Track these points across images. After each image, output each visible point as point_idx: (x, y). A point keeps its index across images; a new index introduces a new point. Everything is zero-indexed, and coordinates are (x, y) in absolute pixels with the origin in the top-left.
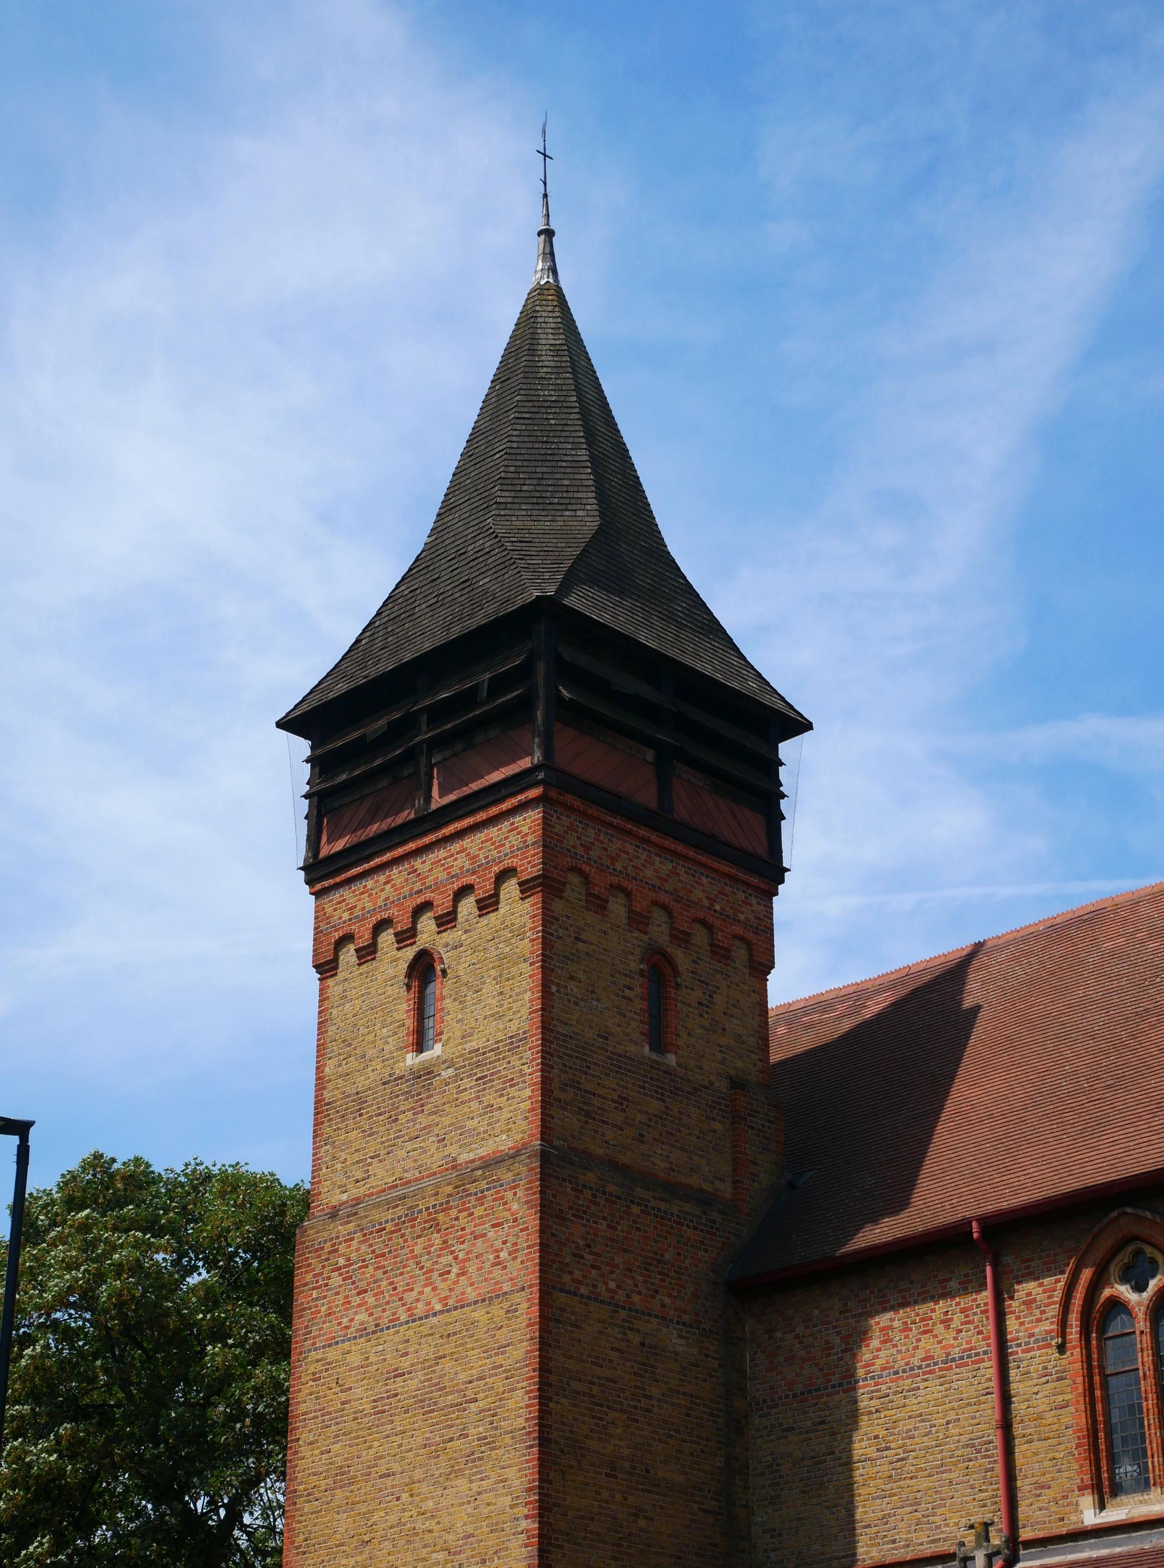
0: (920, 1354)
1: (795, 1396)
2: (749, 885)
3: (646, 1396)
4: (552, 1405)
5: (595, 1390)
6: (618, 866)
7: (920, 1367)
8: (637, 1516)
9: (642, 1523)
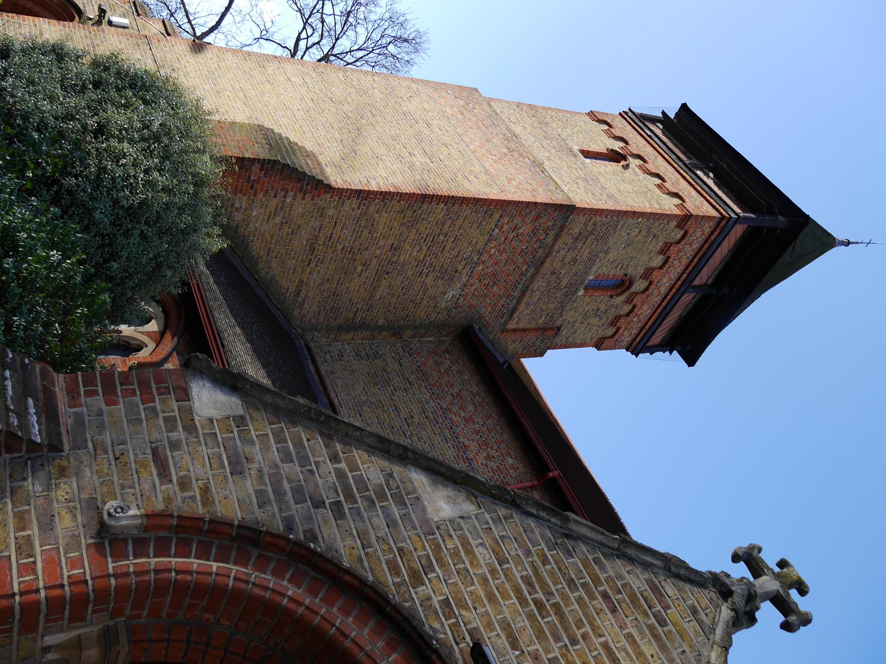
0: (467, 443)
1: (419, 367)
2: (637, 336)
3: (428, 273)
4: (442, 205)
5: (442, 237)
6: (676, 262)
7: (459, 442)
8: (364, 265)
9: (360, 268)
